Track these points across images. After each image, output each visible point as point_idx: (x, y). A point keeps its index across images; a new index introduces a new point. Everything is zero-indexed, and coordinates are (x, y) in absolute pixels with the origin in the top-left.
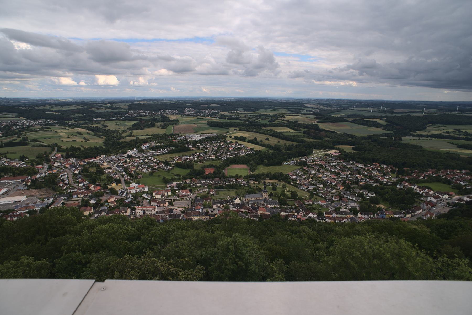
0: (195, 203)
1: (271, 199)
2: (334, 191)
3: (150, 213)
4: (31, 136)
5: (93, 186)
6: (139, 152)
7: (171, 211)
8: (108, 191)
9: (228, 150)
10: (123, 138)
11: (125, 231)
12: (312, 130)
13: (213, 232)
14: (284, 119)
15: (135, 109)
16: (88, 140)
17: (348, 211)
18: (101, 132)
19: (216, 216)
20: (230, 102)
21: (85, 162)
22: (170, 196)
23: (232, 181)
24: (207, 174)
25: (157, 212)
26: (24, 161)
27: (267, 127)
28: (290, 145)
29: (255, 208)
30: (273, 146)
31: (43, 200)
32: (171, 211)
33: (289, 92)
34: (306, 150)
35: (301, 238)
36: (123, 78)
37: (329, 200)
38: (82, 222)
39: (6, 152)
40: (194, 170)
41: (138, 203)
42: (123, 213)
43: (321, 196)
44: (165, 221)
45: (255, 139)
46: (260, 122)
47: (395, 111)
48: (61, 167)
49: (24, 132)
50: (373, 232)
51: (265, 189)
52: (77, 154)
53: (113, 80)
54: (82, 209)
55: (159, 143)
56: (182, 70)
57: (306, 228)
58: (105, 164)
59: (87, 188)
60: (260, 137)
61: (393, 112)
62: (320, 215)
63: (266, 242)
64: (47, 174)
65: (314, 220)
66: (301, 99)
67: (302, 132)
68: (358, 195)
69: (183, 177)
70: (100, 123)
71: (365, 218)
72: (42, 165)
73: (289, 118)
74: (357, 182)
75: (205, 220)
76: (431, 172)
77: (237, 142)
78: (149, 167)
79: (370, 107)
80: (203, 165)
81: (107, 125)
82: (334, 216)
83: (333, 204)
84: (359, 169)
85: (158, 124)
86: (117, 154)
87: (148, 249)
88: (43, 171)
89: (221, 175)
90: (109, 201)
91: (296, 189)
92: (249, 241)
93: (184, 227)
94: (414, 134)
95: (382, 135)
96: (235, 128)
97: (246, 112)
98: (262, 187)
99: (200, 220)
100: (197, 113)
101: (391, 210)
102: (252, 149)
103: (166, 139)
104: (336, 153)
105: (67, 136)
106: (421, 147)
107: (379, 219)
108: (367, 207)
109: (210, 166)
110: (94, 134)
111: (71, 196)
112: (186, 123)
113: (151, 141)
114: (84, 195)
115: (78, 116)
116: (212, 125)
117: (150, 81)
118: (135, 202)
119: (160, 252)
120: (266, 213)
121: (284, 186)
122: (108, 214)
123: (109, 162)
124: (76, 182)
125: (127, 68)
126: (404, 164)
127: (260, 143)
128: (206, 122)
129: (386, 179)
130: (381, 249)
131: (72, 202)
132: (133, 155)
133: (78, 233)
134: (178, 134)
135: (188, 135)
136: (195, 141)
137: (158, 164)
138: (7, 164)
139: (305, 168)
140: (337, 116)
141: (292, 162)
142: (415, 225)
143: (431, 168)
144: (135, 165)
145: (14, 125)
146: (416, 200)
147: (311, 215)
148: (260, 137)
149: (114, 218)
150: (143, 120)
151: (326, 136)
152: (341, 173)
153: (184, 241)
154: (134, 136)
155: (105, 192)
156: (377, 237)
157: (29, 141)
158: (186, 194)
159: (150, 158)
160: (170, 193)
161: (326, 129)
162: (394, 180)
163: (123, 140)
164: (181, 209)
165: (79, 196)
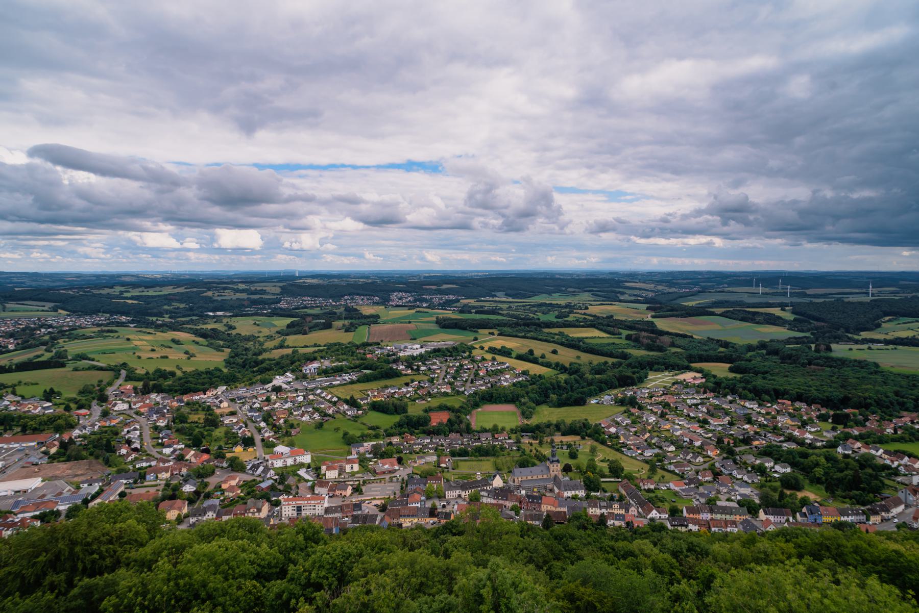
0: (409, 487)
1: (567, 478)
2: (700, 459)
3: (312, 512)
4: (73, 348)
5: (192, 452)
6: (297, 379)
7: (358, 506)
8: (225, 465)
9: (476, 374)
10: (265, 350)
11: (253, 556)
12: (642, 333)
13: (447, 555)
14: (586, 311)
15: (294, 295)
16: (193, 356)
17: (735, 505)
18: (222, 340)
19: (452, 518)
20: (479, 280)
21: (183, 402)
22: (357, 472)
23: (486, 440)
24: (435, 424)
25: (327, 511)
26: (51, 401)
27: (553, 327)
28: (599, 364)
29: (535, 499)
30: (567, 366)
31: (78, 488)
32: (358, 506)
33: (594, 260)
34: (628, 375)
35: (639, 569)
36: (271, 233)
37: (691, 481)
38: (161, 536)
39: (16, 382)
40: (407, 417)
41: (287, 491)
42: (253, 513)
43: (673, 472)
44: (344, 531)
45: (531, 352)
46: (539, 319)
47: (808, 292)
48: (128, 412)
49: (61, 341)
50: (800, 556)
51: (553, 455)
52: (168, 386)
53: (251, 239)
54: (164, 505)
55: (338, 360)
56: (383, 220)
57: (645, 545)
58: (225, 404)
59: (180, 458)
60: (540, 348)
61: (805, 295)
62: (674, 512)
63: (561, 578)
64: (96, 427)
65: (662, 528)
66: (616, 273)
67: (623, 336)
68: (753, 468)
69: (386, 431)
70: (221, 322)
71: (775, 524)
72: (89, 408)
73: (597, 310)
74: (747, 441)
75: (429, 527)
76: (908, 419)
77: (494, 359)
78: (316, 410)
79: (757, 286)
80: (427, 405)
81: (236, 324)
82: (706, 516)
83: (701, 489)
84: (749, 411)
85: (338, 323)
86: (251, 384)
87: (302, 599)
88: (89, 422)
89: (463, 426)
90: (224, 486)
91: (618, 456)
92: (524, 576)
93: (385, 542)
94: (856, 337)
95: (789, 341)
96: (491, 331)
97: (511, 300)
98: (546, 451)
99: (418, 527)
100: (415, 300)
101: (833, 505)
102: (524, 373)
103: (353, 353)
104: (695, 378)
105: (150, 348)
106: (876, 365)
107: (807, 525)
108: (776, 496)
109: (442, 408)
110: (207, 343)
111: (143, 477)
112: (394, 322)
113: (322, 358)
114: (172, 474)
115: (178, 308)
116: (446, 325)
117: (323, 241)
118: (281, 487)
119: (328, 606)
120: (559, 509)
121: (593, 450)
122: (219, 515)
123: (233, 400)
124: (158, 444)
125: (277, 216)
126: (845, 402)
127: (541, 360)
128: (435, 319)
129: (811, 433)
130: (826, 601)
131: (143, 491)
132: (284, 386)
133: (147, 565)
134: (378, 344)
135: (397, 344)
136: (414, 358)
137: (335, 403)
138: (13, 408)
139: (635, 411)
140: (691, 304)
141: (606, 397)
142: (896, 541)
143: (907, 410)
144: (286, 407)
145: (42, 326)
146: (887, 482)
147: (654, 514)
148: (540, 348)
149: (232, 527)
150: (309, 315)
151: (673, 345)
152: (712, 422)
153: (383, 579)
154: (288, 347)
155: (217, 467)
156: (811, 570)
157: (70, 358)
158: (391, 468)
159: (319, 391)
160: (356, 467)
161: (671, 330)
162: (829, 436)
163: (265, 356)
164: (379, 502)
165: (159, 475)
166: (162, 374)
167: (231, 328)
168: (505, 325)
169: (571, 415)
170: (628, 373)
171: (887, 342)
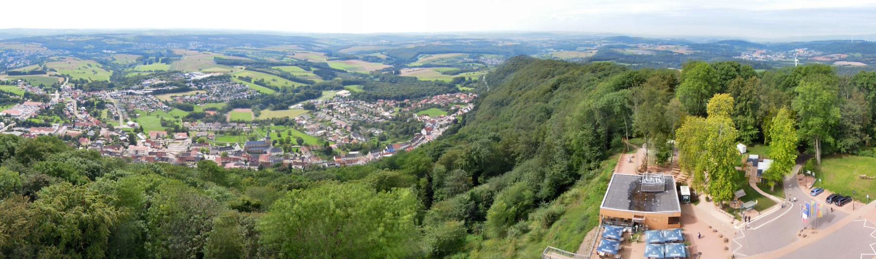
4: (49, 65)
12: (324, 71)
25: (150, 153)
45: (263, 80)
60: (267, 78)
95: (383, 70)
116: (220, 62)
126: (403, 98)
148: (267, 78)
166: (83, 81)
167: (114, 60)
168: (251, 64)
169: (280, 114)
170: (312, 92)
171: (420, 67)
